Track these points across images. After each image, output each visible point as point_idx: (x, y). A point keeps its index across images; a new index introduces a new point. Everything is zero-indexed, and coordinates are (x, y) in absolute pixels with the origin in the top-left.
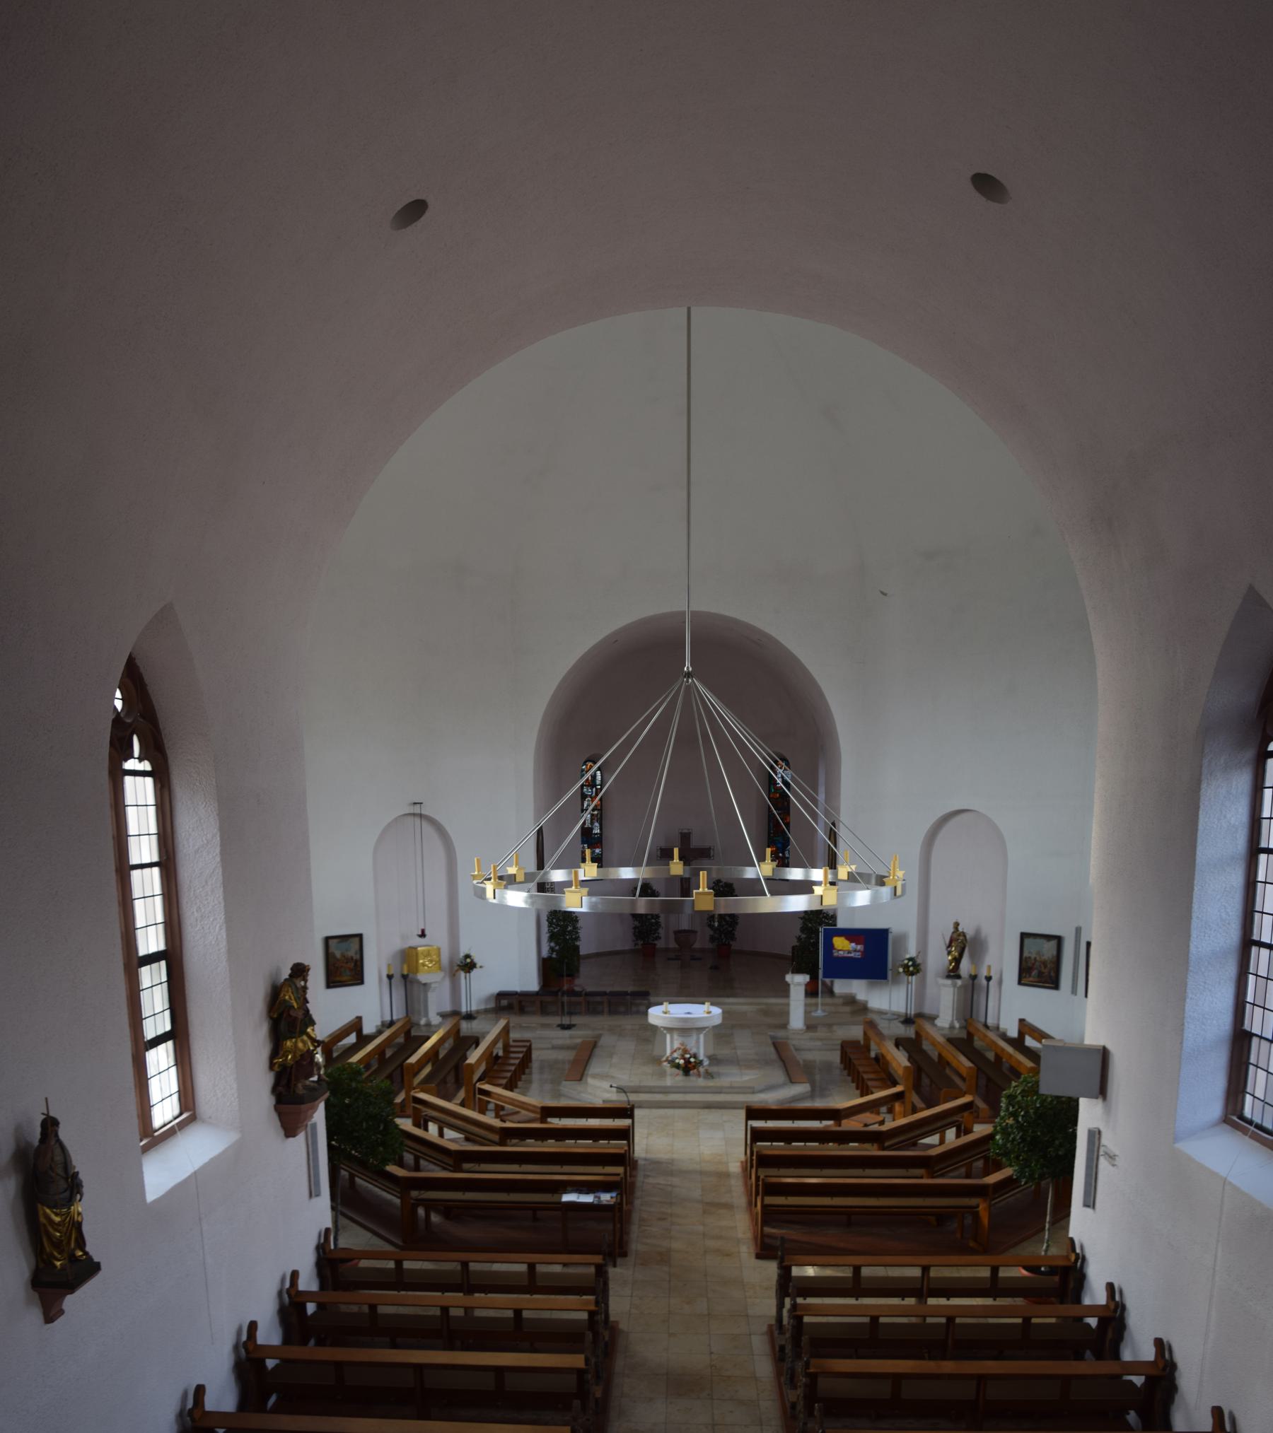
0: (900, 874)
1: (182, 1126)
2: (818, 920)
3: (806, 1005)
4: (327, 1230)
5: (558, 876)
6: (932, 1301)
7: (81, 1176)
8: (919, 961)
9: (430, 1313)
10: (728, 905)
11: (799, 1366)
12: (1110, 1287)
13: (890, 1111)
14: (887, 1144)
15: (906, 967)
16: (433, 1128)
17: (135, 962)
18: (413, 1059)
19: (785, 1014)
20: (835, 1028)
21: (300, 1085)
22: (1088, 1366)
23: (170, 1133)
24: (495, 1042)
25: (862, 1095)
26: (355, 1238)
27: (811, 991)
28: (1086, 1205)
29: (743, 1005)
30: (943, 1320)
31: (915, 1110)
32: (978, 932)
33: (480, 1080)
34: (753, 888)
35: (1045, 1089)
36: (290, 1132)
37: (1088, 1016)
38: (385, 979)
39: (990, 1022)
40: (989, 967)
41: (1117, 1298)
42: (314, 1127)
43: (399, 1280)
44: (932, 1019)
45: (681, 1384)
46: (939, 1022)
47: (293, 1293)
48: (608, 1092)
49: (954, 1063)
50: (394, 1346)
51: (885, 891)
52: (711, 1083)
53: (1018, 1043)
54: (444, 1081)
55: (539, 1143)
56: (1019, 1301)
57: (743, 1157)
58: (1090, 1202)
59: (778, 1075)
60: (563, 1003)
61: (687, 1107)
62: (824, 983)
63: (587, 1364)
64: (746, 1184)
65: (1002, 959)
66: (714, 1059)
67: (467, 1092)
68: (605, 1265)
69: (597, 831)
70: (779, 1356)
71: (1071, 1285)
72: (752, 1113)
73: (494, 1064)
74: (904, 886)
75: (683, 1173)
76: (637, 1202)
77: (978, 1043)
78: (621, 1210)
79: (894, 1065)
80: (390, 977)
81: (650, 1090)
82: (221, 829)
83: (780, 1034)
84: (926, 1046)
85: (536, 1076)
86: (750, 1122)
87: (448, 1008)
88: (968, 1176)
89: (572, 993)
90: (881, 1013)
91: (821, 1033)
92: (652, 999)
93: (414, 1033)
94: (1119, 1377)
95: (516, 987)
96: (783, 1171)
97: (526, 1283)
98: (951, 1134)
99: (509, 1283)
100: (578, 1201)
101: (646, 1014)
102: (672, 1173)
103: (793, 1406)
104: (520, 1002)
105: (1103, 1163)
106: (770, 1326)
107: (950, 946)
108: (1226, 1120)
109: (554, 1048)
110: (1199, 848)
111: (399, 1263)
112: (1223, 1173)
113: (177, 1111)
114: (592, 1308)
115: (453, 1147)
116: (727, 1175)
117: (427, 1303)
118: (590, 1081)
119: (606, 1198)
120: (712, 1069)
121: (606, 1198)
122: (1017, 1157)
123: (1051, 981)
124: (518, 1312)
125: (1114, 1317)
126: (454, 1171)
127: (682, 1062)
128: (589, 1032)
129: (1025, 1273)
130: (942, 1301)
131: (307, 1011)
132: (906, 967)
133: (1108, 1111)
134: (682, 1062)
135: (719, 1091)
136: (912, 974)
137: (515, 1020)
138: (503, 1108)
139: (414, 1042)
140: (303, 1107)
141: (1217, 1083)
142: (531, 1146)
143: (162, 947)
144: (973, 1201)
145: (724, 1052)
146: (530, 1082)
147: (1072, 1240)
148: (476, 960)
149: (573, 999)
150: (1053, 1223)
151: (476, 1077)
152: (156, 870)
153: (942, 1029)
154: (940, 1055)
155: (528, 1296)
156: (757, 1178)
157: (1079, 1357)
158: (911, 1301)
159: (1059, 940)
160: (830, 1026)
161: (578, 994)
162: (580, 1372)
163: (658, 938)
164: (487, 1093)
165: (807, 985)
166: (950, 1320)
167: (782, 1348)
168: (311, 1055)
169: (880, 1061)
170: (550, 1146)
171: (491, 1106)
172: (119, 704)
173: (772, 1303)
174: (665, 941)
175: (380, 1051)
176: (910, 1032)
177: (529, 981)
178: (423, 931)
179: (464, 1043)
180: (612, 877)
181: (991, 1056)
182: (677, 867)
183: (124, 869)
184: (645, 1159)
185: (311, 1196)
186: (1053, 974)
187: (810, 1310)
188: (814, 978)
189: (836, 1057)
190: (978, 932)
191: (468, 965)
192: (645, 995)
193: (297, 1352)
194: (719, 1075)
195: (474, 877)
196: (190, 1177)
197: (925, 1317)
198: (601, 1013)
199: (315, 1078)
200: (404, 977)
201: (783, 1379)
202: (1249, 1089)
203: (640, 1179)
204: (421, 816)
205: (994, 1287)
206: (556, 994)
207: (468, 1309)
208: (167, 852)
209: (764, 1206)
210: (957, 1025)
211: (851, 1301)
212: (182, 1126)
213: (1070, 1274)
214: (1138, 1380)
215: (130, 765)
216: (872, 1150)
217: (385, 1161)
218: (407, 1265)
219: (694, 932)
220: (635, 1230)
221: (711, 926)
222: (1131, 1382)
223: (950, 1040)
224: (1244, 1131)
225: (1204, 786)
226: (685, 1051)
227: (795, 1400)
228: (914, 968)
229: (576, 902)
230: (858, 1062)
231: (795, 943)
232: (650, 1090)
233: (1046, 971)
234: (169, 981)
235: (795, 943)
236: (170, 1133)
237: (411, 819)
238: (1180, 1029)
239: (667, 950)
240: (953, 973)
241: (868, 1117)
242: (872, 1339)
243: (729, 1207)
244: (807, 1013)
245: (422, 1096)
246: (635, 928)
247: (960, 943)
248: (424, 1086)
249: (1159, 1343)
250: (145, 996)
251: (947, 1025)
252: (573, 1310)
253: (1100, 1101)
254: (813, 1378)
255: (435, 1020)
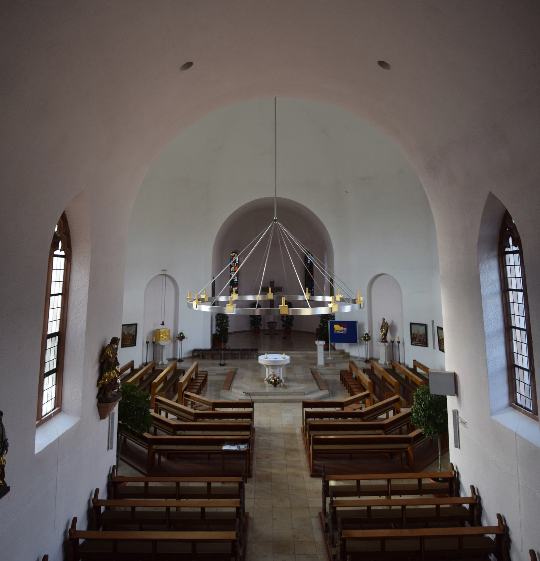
0: (362, 299)
1: (55, 414)
2: (328, 318)
3: (324, 354)
4: (114, 466)
5: (222, 299)
6: (393, 497)
7: (8, 441)
8: (370, 335)
9: (159, 510)
10: (290, 312)
11: (337, 535)
12: (472, 487)
13: (364, 403)
14: (365, 418)
15: (365, 337)
16: (163, 413)
17: (46, 336)
18: (156, 381)
19: (316, 358)
20: (337, 364)
21: (109, 394)
22: (468, 530)
23: (50, 417)
24: (192, 372)
25: (351, 396)
26: (126, 471)
27: (326, 348)
28: (456, 447)
29: (298, 355)
30: (400, 507)
31: (374, 403)
32: (393, 322)
33: (185, 390)
34: (303, 305)
35: (432, 392)
36: (102, 416)
37: (449, 360)
38: (145, 343)
39: (401, 361)
40: (399, 337)
41: (476, 493)
42: (113, 414)
43: (146, 493)
44: (377, 360)
45: (280, 546)
46: (380, 362)
47: (95, 501)
48: (241, 395)
49: (389, 380)
50: (141, 529)
51: (356, 306)
52: (286, 390)
53: (414, 370)
54: (169, 391)
55: (211, 420)
56: (431, 496)
57: (301, 426)
58: (457, 445)
59: (315, 386)
60: (221, 354)
61: (277, 401)
62: (331, 345)
63: (237, 537)
64: (304, 439)
65: (403, 334)
66: (287, 380)
67: (179, 396)
68: (243, 482)
69: (236, 280)
70: (325, 529)
71: (454, 487)
72: (306, 405)
73: (191, 381)
74: (364, 304)
75: (275, 434)
76: (255, 449)
77: (397, 371)
78: (249, 453)
79: (364, 381)
80: (147, 343)
81: (260, 394)
82: (90, 281)
83: (314, 367)
84: (376, 372)
85: (208, 388)
86: (305, 409)
87: (171, 357)
88: (401, 433)
89: (225, 349)
90: (355, 358)
91: (331, 367)
92: (259, 352)
93: (156, 368)
94: (482, 535)
95: (201, 346)
96: (321, 433)
97: (206, 493)
98: (391, 413)
99: (198, 494)
100: (223, 450)
101: (257, 359)
102: (270, 434)
103: (335, 557)
104: (203, 354)
105: (461, 425)
106: (320, 513)
107: (382, 328)
108: (510, 405)
109: (217, 374)
110: (482, 289)
111: (146, 484)
112: (514, 430)
113: (53, 407)
114: (238, 505)
115: (173, 423)
116: (293, 435)
117: (158, 505)
118: (233, 390)
119: (243, 447)
120: (286, 384)
121: (243, 447)
122: (423, 424)
123: (424, 343)
124: (203, 509)
125: (476, 503)
126: (173, 435)
127: (273, 381)
128: (233, 367)
129: (432, 481)
130: (397, 497)
131: (117, 359)
132: (365, 337)
133: (459, 401)
134: (273, 381)
135: (290, 394)
136: (367, 340)
137: (201, 362)
138: (194, 403)
139: (156, 372)
140: (110, 404)
141: (504, 389)
142: (207, 422)
143: (57, 330)
144: (406, 446)
145: (291, 376)
146: (206, 391)
147: (452, 464)
148: (185, 335)
149: (226, 352)
150: (442, 455)
151: (183, 389)
152: (60, 297)
153: (381, 364)
154: (382, 377)
155: (207, 500)
156: (310, 436)
157: (463, 525)
158: (383, 497)
159: (426, 326)
160: (334, 364)
161: (228, 350)
162: (233, 541)
163: (261, 325)
164: (187, 396)
165: (324, 346)
166: (403, 507)
167: (327, 525)
168: (116, 379)
169: (358, 380)
170: (216, 422)
171: (189, 403)
172: (56, 229)
173: (321, 500)
174: (264, 326)
175: (141, 377)
176: (368, 366)
177: (208, 345)
178: (163, 322)
179: (179, 372)
180: (244, 299)
181: (403, 376)
182: (270, 296)
183: (48, 295)
184: (258, 428)
185: (108, 449)
186: (425, 340)
187: (338, 502)
188: (327, 342)
189: (338, 378)
190: (393, 322)
191: (181, 337)
192: (256, 350)
193: (94, 534)
194: (289, 386)
195: (188, 299)
196: (56, 440)
197: (390, 506)
198: (238, 358)
199: (116, 391)
200: (154, 343)
201: (328, 542)
202: (518, 391)
203: (256, 437)
204: (166, 275)
205: (420, 490)
206: (218, 350)
207: (178, 508)
208: (507, 312)
209: (313, 450)
210: (388, 363)
211: (357, 498)
212: (55, 414)
213: (453, 482)
214: (493, 537)
215: (57, 252)
216: (358, 422)
217: (144, 431)
218: (151, 484)
219: (276, 323)
220: (255, 463)
221: (283, 320)
222: (489, 538)
223: (385, 369)
224: (520, 411)
225: (480, 265)
226: (274, 376)
227: (335, 554)
228: (368, 338)
229: (230, 310)
230: (348, 380)
231: (318, 327)
232: (260, 394)
233: (422, 339)
234: (58, 346)
235: (318, 327)
236: (50, 417)
237: (161, 277)
238: (486, 365)
239: (264, 330)
240: (384, 340)
241: (354, 406)
242: (368, 519)
243: (297, 451)
244: (325, 358)
245: (160, 398)
246: (251, 321)
247: (386, 327)
248: (160, 393)
249: (499, 516)
250: (48, 352)
251: (383, 363)
252: (227, 507)
253: (456, 397)
254: (344, 540)
255: (166, 362)
